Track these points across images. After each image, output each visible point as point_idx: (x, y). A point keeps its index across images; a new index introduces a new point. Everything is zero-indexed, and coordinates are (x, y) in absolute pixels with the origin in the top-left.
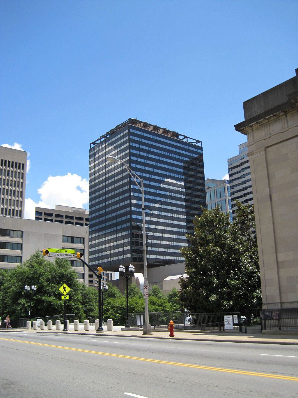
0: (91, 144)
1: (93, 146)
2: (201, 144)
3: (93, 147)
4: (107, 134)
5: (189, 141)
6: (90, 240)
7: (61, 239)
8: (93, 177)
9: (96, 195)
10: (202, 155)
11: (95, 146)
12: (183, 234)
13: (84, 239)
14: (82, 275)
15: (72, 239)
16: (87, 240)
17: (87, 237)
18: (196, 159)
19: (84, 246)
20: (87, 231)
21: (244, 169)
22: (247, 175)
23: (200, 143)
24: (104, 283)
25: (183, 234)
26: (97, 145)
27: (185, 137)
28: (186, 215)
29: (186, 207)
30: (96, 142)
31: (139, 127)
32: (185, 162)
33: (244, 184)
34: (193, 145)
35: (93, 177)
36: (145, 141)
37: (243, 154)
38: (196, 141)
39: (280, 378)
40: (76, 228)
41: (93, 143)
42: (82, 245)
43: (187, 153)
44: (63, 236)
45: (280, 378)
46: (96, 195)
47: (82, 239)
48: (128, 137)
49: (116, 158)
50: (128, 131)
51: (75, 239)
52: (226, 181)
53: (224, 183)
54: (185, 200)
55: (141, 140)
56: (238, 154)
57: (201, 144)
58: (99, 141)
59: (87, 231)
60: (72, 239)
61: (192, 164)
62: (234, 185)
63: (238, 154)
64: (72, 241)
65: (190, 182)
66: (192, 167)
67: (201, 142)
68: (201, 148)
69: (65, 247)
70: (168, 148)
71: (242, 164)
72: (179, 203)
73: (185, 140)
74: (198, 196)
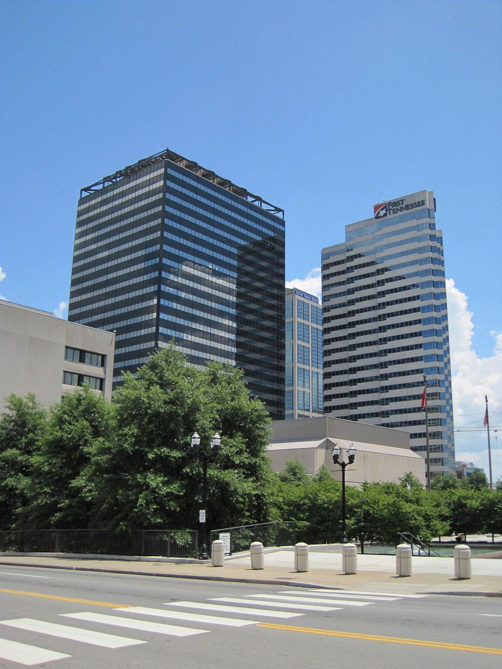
0: (82, 190)
1: (85, 194)
2: (283, 215)
4: (119, 173)
5: (265, 207)
6: (117, 358)
7: (62, 374)
10: (283, 234)
11: (89, 195)
15: (82, 355)
16: (110, 360)
17: (110, 352)
18: (272, 239)
19: (105, 372)
20: (111, 343)
21: (352, 267)
23: (282, 213)
26: (93, 193)
27: (258, 198)
30: (92, 189)
31: (181, 165)
32: (239, 247)
33: (350, 294)
34: (270, 215)
36: (191, 194)
37: (351, 242)
38: (274, 209)
39: (304, 631)
41: (86, 190)
42: (101, 369)
43: (260, 228)
44: (64, 371)
45: (304, 631)
48: (162, 183)
49: (215, 183)
50: (163, 170)
51: (88, 355)
52: (296, 291)
53: (293, 293)
55: (184, 191)
56: (344, 241)
57: (283, 215)
58: (100, 187)
59: (111, 343)
60: (82, 355)
61: (251, 252)
62: (331, 295)
63: (344, 241)
64: (82, 360)
66: (249, 257)
67: (283, 211)
68: (282, 223)
70: (229, 213)
71: (351, 259)
73: (257, 203)
74: (271, 307)
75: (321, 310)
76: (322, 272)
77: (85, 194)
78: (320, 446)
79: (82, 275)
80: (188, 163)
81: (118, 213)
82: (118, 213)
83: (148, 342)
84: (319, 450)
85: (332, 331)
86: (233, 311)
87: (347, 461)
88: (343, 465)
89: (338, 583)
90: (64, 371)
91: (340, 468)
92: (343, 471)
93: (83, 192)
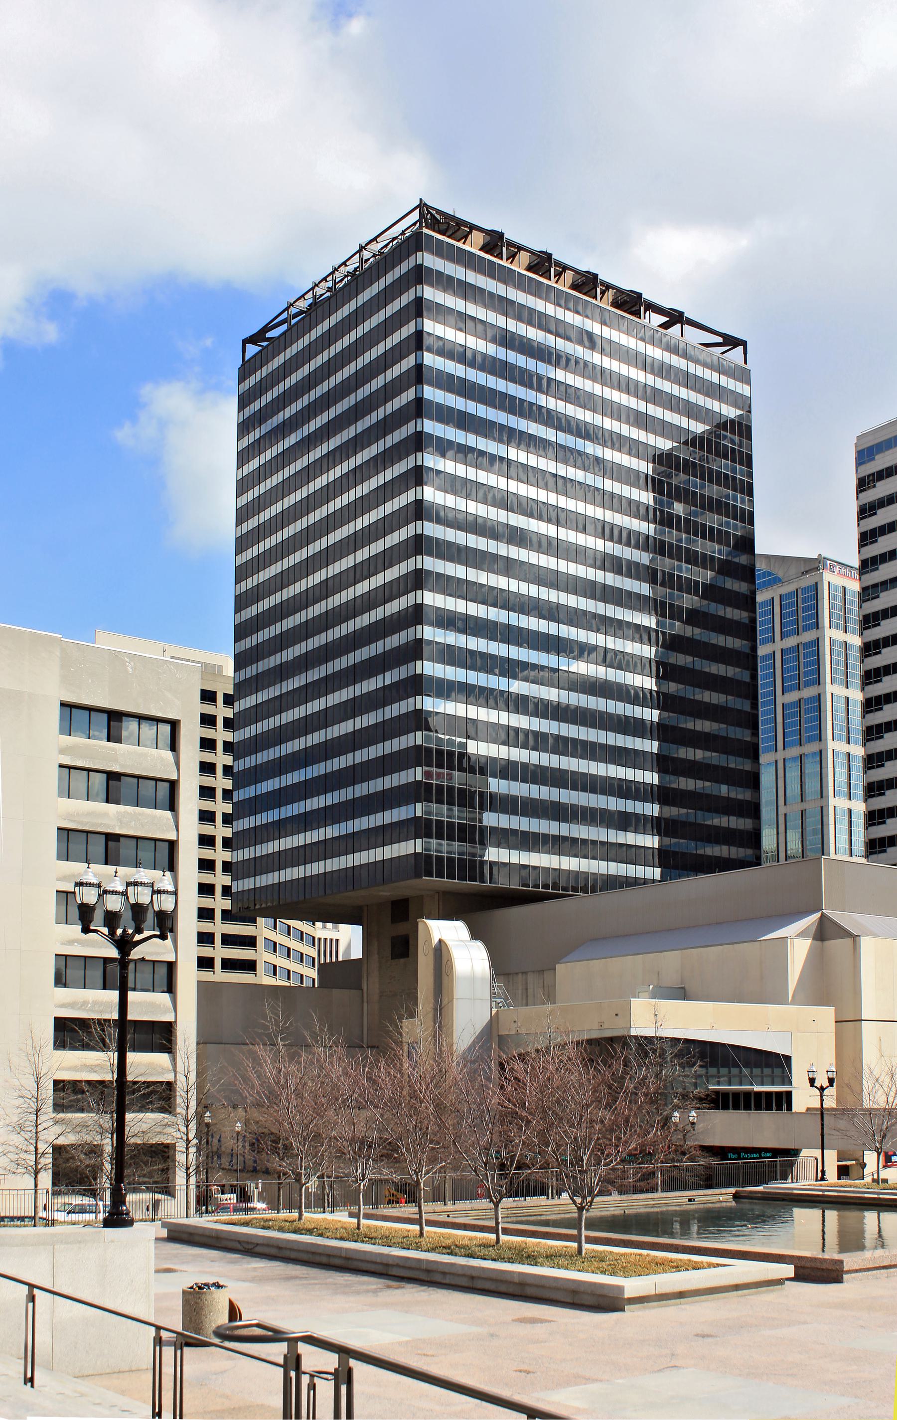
0: (245, 342)
1: (252, 350)
3: (255, 356)
7: (55, 713)
8: (252, 553)
9: (263, 666)
11: (261, 351)
12: (634, 727)
13: (174, 725)
14: (163, 971)
22: (887, 590)
24: (275, 967)
25: (634, 727)
26: (267, 346)
28: (659, 772)
29: (662, 731)
35: (252, 553)
38: (720, 340)
40: (134, 669)
41: (252, 340)
44: (63, 704)
46: (263, 666)
47: (166, 729)
54: (662, 795)
65: (676, 494)
69: (158, 1311)
72: (626, 460)
75: (856, 595)
76: (860, 607)
77: (252, 350)
78: (801, 935)
79: (323, 642)
80: (535, 258)
81: (324, 388)
82: (324, 388)
83: (340, 656)
84: (796, 941)
85: (884, 647)
86: (652, 715)
87: (826, 1084)
88: (822, 1089)
89: (822, 808)
90: (63, 704)
91: (818, 1092)
92: (821, 1096)
93: (248, 346)
